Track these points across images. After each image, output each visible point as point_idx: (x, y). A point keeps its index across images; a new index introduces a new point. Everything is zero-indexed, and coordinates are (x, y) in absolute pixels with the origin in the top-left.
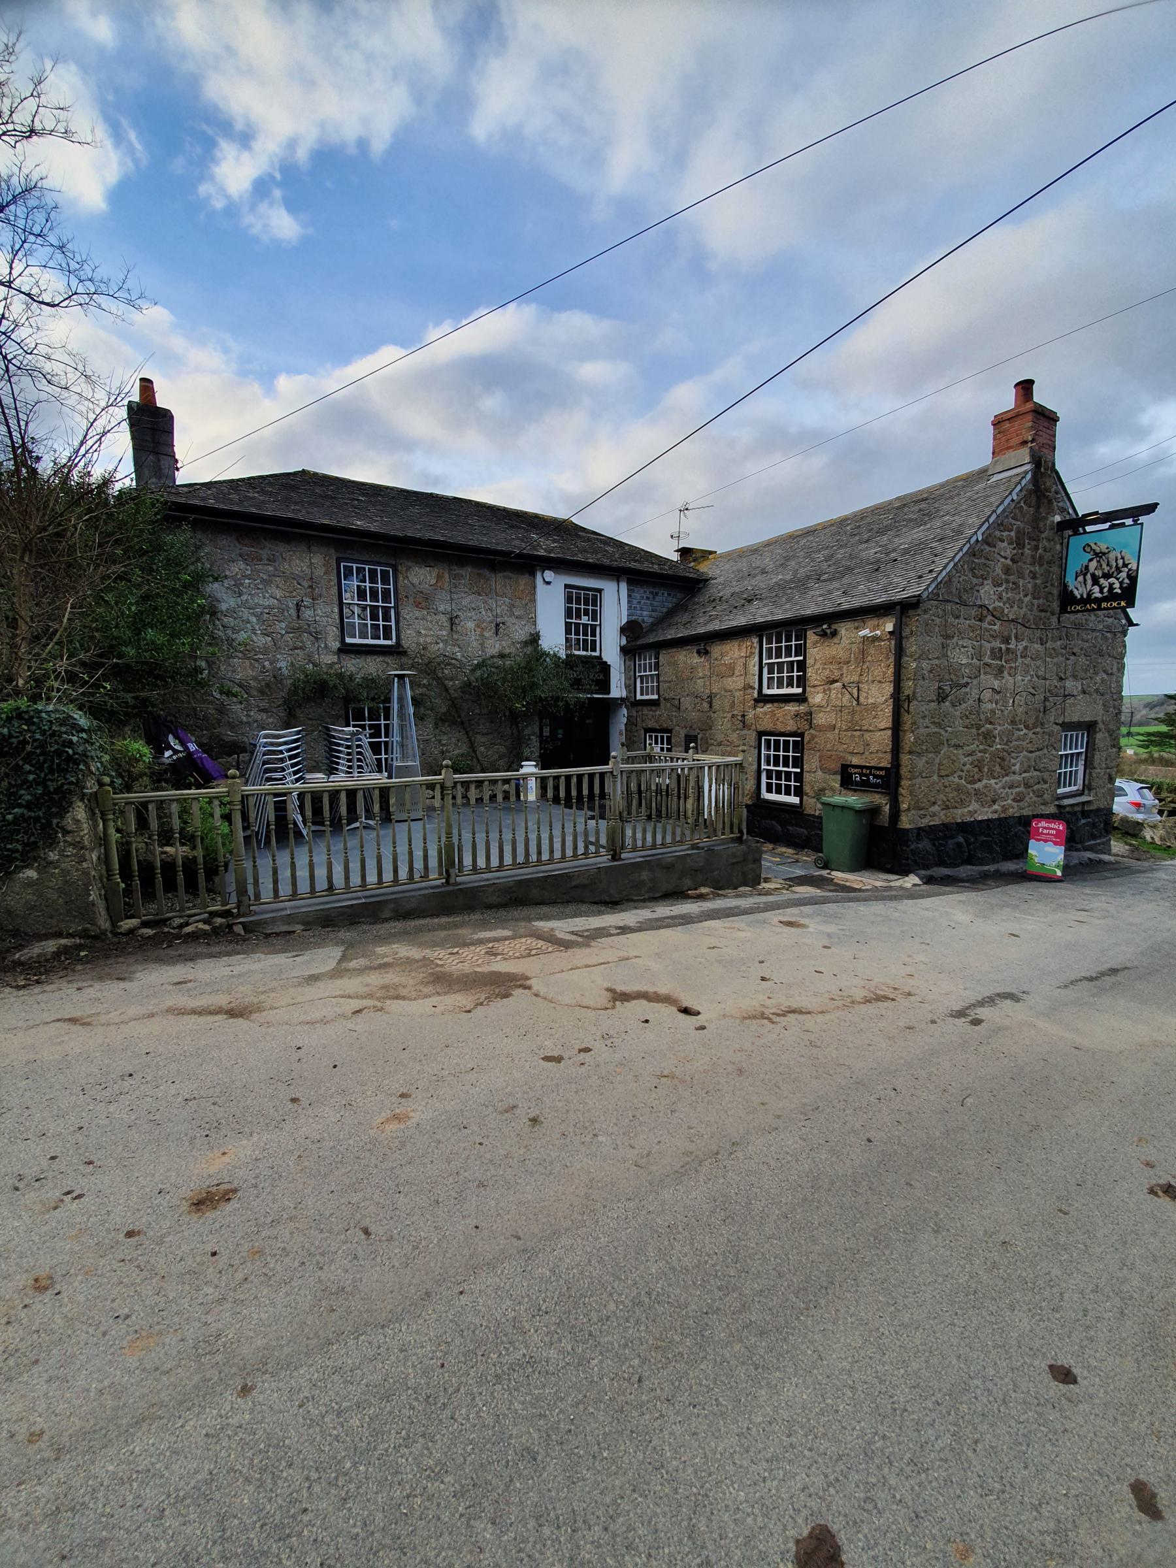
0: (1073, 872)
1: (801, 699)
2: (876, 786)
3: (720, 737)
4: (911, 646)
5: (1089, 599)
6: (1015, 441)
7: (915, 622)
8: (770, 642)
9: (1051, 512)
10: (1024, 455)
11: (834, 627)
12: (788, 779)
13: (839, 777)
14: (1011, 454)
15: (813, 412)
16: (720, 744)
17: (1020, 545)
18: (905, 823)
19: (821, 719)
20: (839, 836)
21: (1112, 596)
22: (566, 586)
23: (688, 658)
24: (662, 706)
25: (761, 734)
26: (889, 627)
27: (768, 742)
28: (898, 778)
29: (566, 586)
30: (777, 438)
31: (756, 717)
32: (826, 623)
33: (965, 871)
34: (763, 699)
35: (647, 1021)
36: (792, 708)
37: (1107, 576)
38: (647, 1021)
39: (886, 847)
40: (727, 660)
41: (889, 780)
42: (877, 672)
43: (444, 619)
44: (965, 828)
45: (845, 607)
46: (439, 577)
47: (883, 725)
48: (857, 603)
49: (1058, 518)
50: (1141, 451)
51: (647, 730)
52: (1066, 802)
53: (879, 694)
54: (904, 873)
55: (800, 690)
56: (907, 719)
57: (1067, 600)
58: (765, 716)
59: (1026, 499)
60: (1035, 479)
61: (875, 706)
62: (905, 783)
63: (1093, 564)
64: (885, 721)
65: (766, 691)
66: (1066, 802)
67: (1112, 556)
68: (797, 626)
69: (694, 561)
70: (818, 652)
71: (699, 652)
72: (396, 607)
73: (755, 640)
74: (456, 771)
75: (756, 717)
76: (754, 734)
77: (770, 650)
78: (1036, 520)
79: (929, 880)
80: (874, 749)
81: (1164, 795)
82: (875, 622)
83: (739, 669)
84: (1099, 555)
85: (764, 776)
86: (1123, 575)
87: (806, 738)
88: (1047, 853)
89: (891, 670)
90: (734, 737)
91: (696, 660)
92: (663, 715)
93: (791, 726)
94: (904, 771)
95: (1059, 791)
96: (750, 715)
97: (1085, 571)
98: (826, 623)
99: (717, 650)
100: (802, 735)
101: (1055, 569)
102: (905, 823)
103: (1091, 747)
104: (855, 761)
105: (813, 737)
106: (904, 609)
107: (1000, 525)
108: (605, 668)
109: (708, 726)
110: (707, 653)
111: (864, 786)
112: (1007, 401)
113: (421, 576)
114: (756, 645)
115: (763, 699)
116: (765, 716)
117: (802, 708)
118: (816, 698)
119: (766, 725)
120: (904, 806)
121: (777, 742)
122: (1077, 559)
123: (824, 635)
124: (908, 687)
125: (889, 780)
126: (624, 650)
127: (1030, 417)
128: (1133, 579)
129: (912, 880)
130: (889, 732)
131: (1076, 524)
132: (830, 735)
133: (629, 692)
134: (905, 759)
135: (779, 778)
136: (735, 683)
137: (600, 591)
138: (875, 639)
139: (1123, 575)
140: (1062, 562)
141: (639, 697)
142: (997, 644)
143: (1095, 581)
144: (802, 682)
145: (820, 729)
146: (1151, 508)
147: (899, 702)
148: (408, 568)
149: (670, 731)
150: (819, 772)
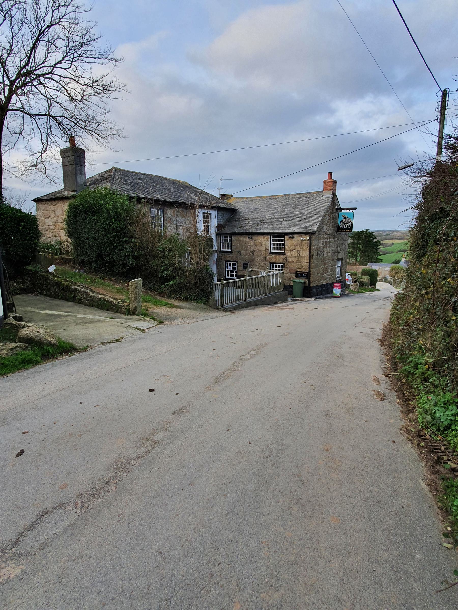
0: (343, 295)
1: (284, 254)
2: (304, 276)
3: (257, 264)
4: (313, 243)
5: (343, 229)
6: (328, 188)
7: (314, 237)
8: (273, 237)
9: (335, 206)
10: (331, 192)
11: (293, 236)
12: (233, 272)
13: (295, 275)
14: (327, 191)
15: (193, 75)
16: (257, 266)
17: (330, 216)
18: (312, 285)
19: (289, 259)
20: (298, 290)
21: (348, 229)
22: (203, 213)
23: (245, 239)
24: (233, 253)
25: (271, 263)
26: (308, 238)
27: (273, 266)
28: (310, 274)
29: (203, 213)
30: (175, 86)
31: (270, 258)
32: (292, 234)
33: (321, 296)
34: (271, 253)
35: (22, 452)
36: (281, 256)
37: (347, 223)
38: (22, 452)
39: (308, 292)
40: (259, 241)
41: (308, 275)
42: (305, 248)
43: (175, 226)
44: (321, 286)
45: (296, 231)
46: (174, 212)
47: (306, 262)
48: (299, 231)
49: (336, 207)
50: (332, 121)
51: (226, 261)
52: (338, 279)
53: (305, 254)
54: (312, 297)
55: (283, 251)
56: (312, 260)
57: (339, 228)
58: (273, 258)
59: (331, 204)
60: (333, 198)
61: (304, 257)
62: (311, 276)
63: (344, 220)
64: (307, 260)
65: (272, 251)
66: (338, 279)
67: (348, 219)
68: (283, 234)
69: (227, 199)
70: (288, 241)
71: (249, 238)
72: (163, 223)
73: (269, 236)
74: (249, 276)
75: (270, 258)
76: (269, 263)
77: (273, 240)
78: (333, 208)
79: (316, 299)
80: (304, 267)
81: (353, 276)
82: (304, 236)
83: (263, 244)
84: (345, 218)
85: (227, 272)
86: (350, 224)
87: (285, 264)
88: (337, 291)
89: (309, 248)
90: (262, 264)
91: (248, 240)
92: (234, 256)
93: (281, 261)
94: (311, 273)
95: (337, 276)
96: (268, 257)
97: (342, 222)
98: (292, 234)
99: (256, 238)
100: (284, 264)
101: (336, 220)
102: (312, 285)
103: (342, 264)
104: (299, 270)
105: (287, 264)
106: (311, 234)
107: (327, 212)
108: (212, 240)
109: (252, 260)
110: (252, 238)
111: (302, 277)
112: (326, 177)
113: (170, 212)
114: (270, 238)
115: (271, 253)
116: (273, 258)
117: (284, 256)
118: (288, 254)
119: (273, 260)
120: (312, 281)
121: (276, 266)
122: (341, 218)
123: (291, 237)
124: (312, 253)
125: (308, 275)
126: (217, 234)
127: (332, 183)
128: (352, 225)
129: (313, 299)
130: (308, 263)
131: (340, 209)
132: (292, 264)
133: (218, 248)
134: (312, 270)
135: (231, 272)
136: (262, 248)
137: (210, 214)
138: (304, 240)
139: (350, 224)
140: (337, 217)
141: (222, 250)
142: (326, 241)
143: (344, 225)
144: (284, 249)
145: (289, 262)
146: (355, 209)
147: (311, 257)
148: (167, 210)
149: (237, 262)
150: (289, 274)
